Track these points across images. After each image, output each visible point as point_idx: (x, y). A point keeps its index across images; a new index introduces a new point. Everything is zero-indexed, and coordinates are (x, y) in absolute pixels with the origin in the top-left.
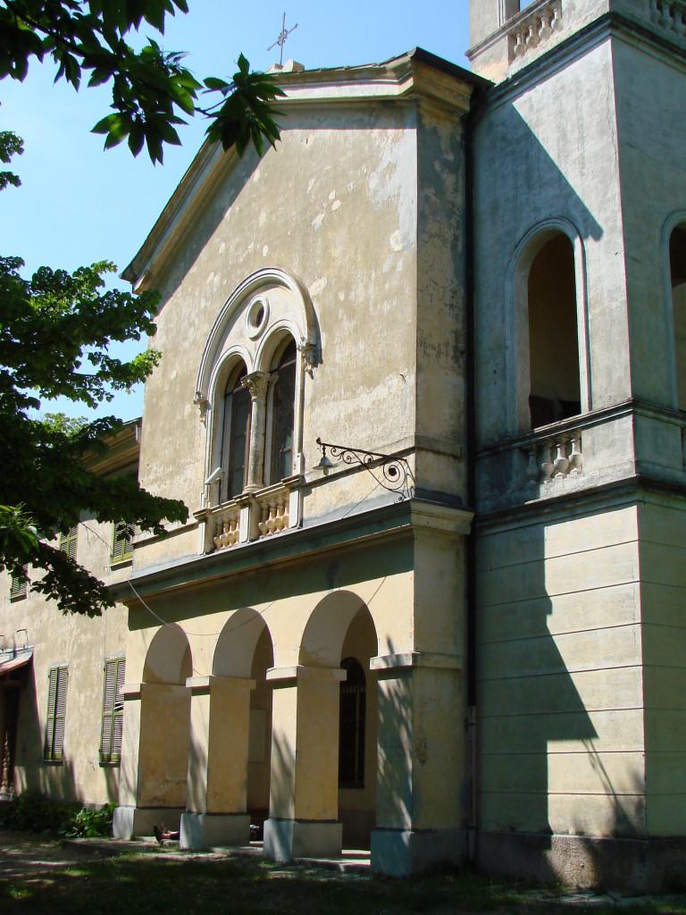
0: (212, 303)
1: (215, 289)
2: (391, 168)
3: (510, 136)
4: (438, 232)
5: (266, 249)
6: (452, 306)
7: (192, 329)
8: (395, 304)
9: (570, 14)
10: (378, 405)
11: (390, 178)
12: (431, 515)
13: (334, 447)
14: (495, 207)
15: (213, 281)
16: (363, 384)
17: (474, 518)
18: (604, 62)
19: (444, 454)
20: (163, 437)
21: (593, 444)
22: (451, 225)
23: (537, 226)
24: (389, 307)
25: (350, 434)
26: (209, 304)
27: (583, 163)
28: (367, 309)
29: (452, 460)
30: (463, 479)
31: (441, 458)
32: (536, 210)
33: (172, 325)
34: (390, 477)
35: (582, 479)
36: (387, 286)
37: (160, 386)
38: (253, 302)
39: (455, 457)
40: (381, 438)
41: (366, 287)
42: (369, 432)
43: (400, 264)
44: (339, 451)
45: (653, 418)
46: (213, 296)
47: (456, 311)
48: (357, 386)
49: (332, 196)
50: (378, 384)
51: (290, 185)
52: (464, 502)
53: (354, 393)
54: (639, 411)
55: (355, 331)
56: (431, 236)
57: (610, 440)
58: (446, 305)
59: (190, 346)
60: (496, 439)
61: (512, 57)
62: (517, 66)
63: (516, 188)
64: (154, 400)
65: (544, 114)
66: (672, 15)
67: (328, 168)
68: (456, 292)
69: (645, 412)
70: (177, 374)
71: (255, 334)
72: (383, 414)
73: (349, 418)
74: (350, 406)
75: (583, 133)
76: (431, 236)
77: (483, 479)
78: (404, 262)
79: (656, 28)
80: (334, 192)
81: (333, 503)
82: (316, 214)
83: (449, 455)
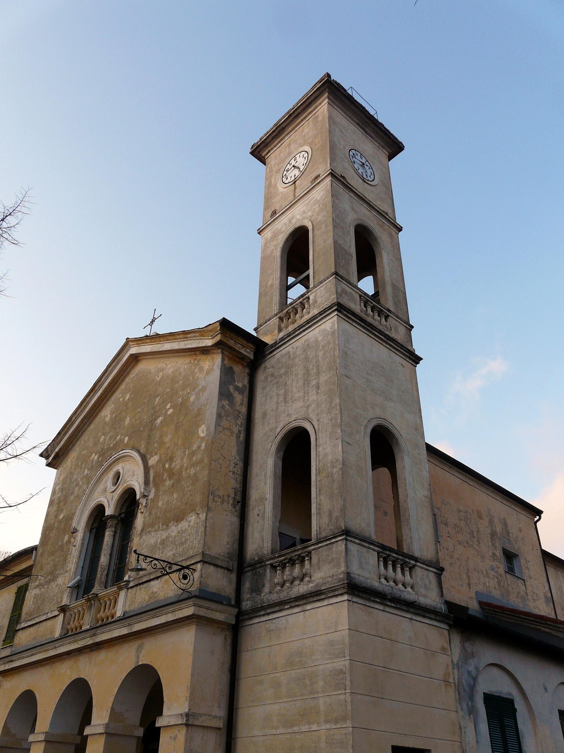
0: (91, 472)
1: (94, 463)
2: (204, 389)
3: (276, 374)
4: (228, 427)
5: (127, 438)
6: (234, 472)
7: (77, 488)
8: (198, 469)
9: (314, 305)
10: (182, 534)
11: (202, 394)
12: (208, 608)
13: (146, 556)
14: (265, 415)
15: (94, 458)
16: (174, 520)
17: (238, 613)
18: (332, 330)
19: (221, 567)
20: (48, 557)
21: (319, 561)
22: (237, 424)
23: (289, 425)
24: (194, 471)
25: (162, 554)
26: (89, 472)
27: (318, 387)
28: (181, 472)
29: (226, 572)
30: (234, 586)
31: (219, 569)
32: (289, 415)
33: (66, 486)
34: (183, 581)
35: (311, 585)
36: (194, 458)
37: (53, 523)
38: (115, 470)
39: (229, 570)
40: (180, 555)
41: (182, 459)
42: (174, 551)
43: (204, 444)
44: (149, 560)
45: (359, 544)
46: (92, 467)
47: (236, 476)
48: (170, 522)
49: (168, 406)
50: (183, 520)
51: (145, 401)
52: (233, 602)
53: (168, 526)
54: (349, 538)
55: (172, 486)
56: (224, 429)
57: (330, 558)
58: (230, 471)
59: (74, 499)
60: (256, 559)
61: (280, 330)
62: (281, 335)
63: (278, 403)
64: (48, 532)
65: (297, 360)
66: (372, 311)
67: (168, 390)
68: (237, 464)
69: (353, 540)
70: (64, 516)
71: (113, 490)
72: (184, 539)
73: (163, 542)
74: (164, 535)
75: (319, 370)
76: (224, 429)
77: (247, 585)
78: (206, 443)
79: (363, 315)
80: (170, 404)
81: (147, 600)
82: (158, 417)
83: (224, 568)
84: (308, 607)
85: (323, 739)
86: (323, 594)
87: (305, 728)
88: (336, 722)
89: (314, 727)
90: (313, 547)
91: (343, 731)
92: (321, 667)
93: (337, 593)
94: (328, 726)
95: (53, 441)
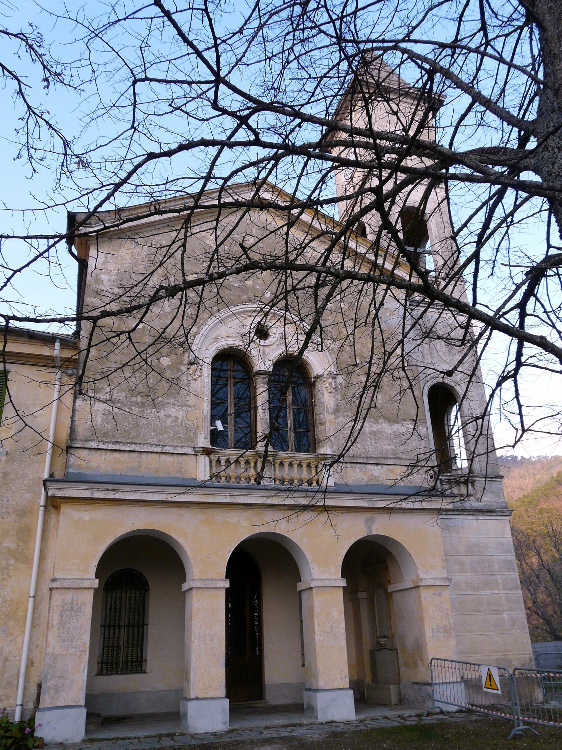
35: (481, 504)
84: (481, 517)
85: (503, 598)
86: (495, 512)
87: (488, 592)
88: (511, 590)
89: (496, 592)
90: (478, 479)
91: (517, 595)
92: (495, 557)
93: (505, 514)
94: (506, 592)
95: (106, 212)
